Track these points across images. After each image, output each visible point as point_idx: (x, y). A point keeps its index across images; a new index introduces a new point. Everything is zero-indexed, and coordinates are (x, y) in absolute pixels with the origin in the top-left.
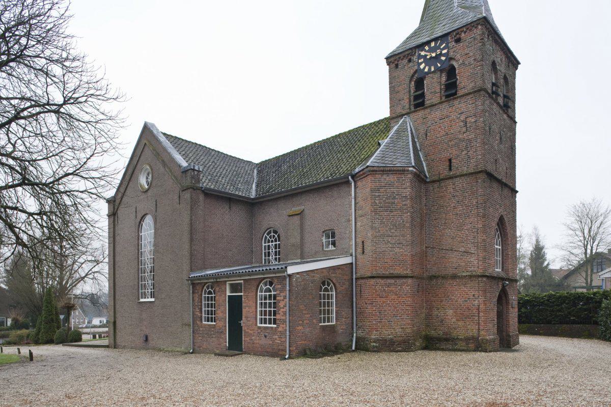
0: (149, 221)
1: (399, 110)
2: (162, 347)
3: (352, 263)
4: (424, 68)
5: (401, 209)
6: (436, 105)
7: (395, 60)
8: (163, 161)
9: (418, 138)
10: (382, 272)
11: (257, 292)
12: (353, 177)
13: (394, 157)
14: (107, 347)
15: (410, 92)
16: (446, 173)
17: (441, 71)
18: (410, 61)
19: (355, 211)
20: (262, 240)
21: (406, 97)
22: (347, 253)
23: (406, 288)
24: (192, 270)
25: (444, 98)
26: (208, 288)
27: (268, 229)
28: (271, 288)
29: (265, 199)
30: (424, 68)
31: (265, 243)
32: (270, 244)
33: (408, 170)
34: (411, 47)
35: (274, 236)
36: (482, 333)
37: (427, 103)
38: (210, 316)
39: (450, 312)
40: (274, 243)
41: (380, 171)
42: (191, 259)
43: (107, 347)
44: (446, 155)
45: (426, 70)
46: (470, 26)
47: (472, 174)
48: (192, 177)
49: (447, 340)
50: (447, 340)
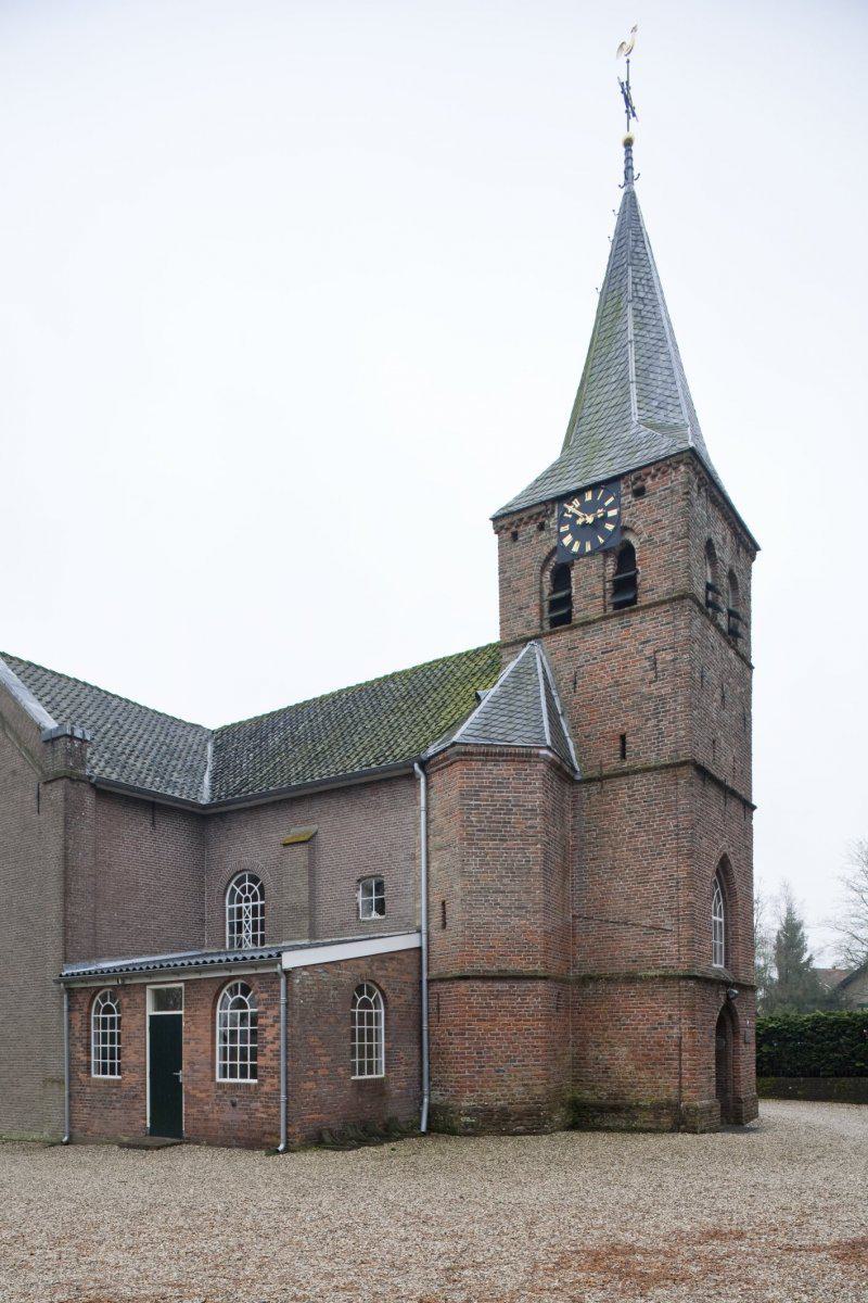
1: (519, 630)
3: (420, 949)
5: (523, 836)
6: (594, 622)
7: (512, 524)
9: (556, 689)
11: (214, 1008)
12: (423, 765)
16: (613, 763)
17: (606, 553)
18: (541, 527)
19: (427, 837)
20: (225, 894)
22: (410, 927)
23: (535, 1002)
24: (66, 960)
25: (610, 610)
27: (238, 873)
28: (114, 1006)
29: (232, 807)
31: (231, 902)
32: (243, 905)
33: (538, 755)
34: (545, 499)
35: (251, 889)
36: (687, 1093)
37: (577, 616)
39: (623, 1051)
40: (251, 904)
41: (480, 754)
42: (65, 934)
44: (616, 726)
48: (69, 754)
49: (616, 1109)
50: (616, 1109)
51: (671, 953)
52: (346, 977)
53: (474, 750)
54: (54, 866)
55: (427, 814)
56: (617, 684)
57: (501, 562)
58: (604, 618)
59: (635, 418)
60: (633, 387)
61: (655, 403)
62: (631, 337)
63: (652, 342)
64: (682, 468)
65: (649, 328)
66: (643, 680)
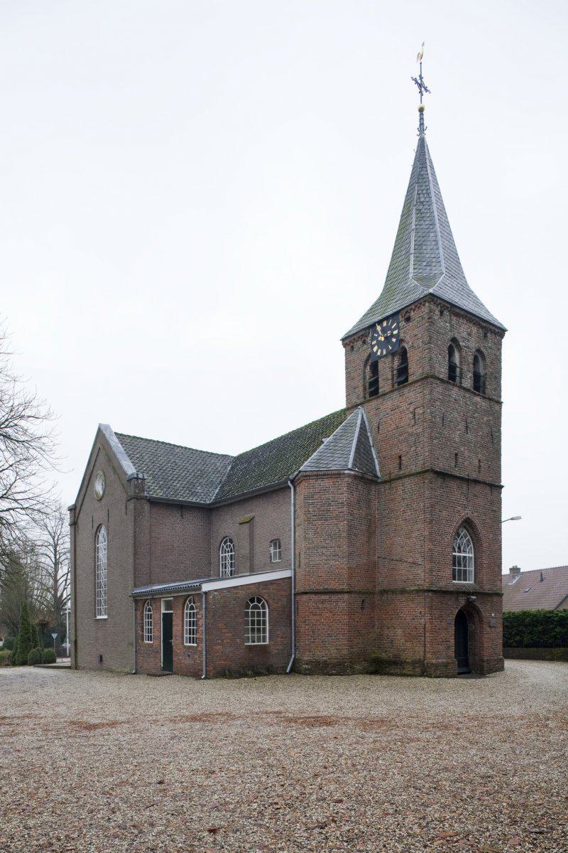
0: (103, 531)
1: (355, 401)
2: (114, 668)
4: (377, 351)
5: (337, 517)
6: (387, 394)
7: (350, 342)
8: (113, 467)
9: (371, 432)
10: (315, 587)
11: (183, 610)
12: (292, 482)
13: (331, 459)
14: (69, 668)
15: (364, 378)
16: (396, 472)
17: (393, 354)
18: (364, 342)
19: (295, 519)
21: (360, 384)
22: (287, 567)
23: (342, 605)
24: (136, 586)
25: (396, 386)
26: (190, 603)
27: (224, 538)
28: (260, 605)
29: (222, 504)
30: (377, 351)
31: (222, 553)
32: (227, 554)
33: (344, 474)
34: (364, 327)
35: (230, 546)
36: (428, 655)
38: (192, 636)
39: (399, 632)
41: (314, 476)
42: (135, 573)
43: (69, 668)
44: (396, 451)
45: (379, 353)
46: (418, 303)
47: (419, 473)
48: (136, 487)
49: (395, 663)
50: (395, 663)
51: (420, 577)
52: (242, 593)
53: (310, 474)
54: (131, 541)
55: (295, 507)
56: (397, 427)
57: (346, 363)
58: (392, 391)
59: (411, 275)
60: (412, 256)
61: (424, 264)
62: (414, 227)
63: (426, 227)
64: (427, 304)
65: (425, 219)
66: (409, 425)
